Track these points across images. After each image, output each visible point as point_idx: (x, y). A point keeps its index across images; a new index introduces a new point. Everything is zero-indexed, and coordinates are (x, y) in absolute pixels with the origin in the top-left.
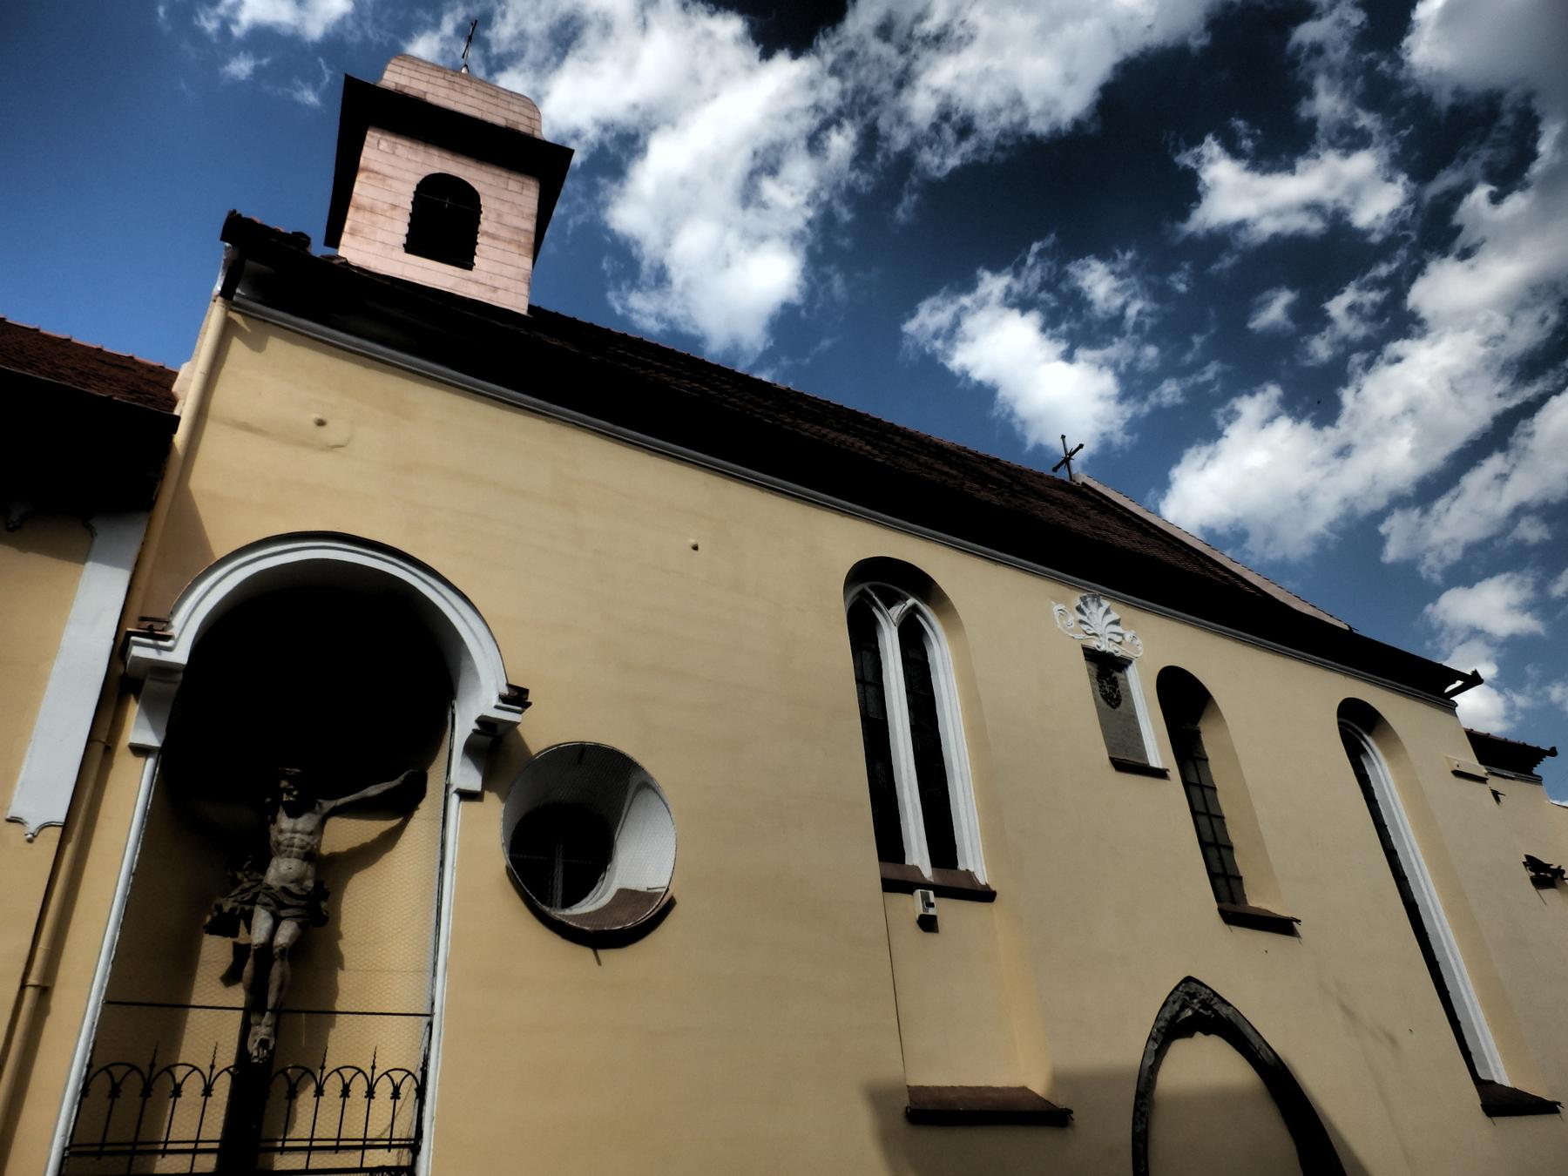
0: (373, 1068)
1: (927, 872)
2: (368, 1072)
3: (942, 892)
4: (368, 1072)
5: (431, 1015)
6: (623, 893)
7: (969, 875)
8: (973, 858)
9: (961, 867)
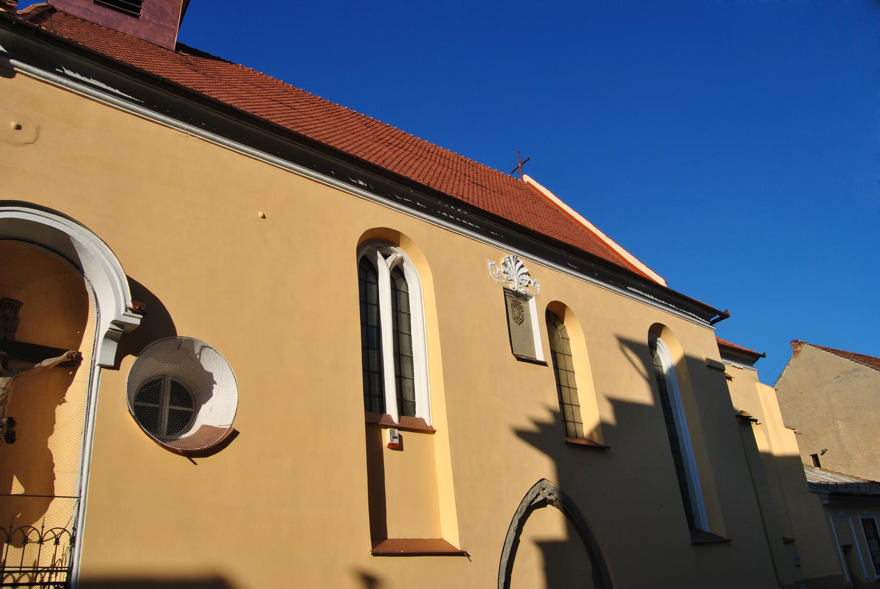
0: (43, 527)
1: (395, 419)
2: (40, 530)
3: (400, 429)
4: (40, 530)
5: (80, 497)
6: (203, 427)
7: (422, 420)
8: (421, 412)
9: (417, 416)
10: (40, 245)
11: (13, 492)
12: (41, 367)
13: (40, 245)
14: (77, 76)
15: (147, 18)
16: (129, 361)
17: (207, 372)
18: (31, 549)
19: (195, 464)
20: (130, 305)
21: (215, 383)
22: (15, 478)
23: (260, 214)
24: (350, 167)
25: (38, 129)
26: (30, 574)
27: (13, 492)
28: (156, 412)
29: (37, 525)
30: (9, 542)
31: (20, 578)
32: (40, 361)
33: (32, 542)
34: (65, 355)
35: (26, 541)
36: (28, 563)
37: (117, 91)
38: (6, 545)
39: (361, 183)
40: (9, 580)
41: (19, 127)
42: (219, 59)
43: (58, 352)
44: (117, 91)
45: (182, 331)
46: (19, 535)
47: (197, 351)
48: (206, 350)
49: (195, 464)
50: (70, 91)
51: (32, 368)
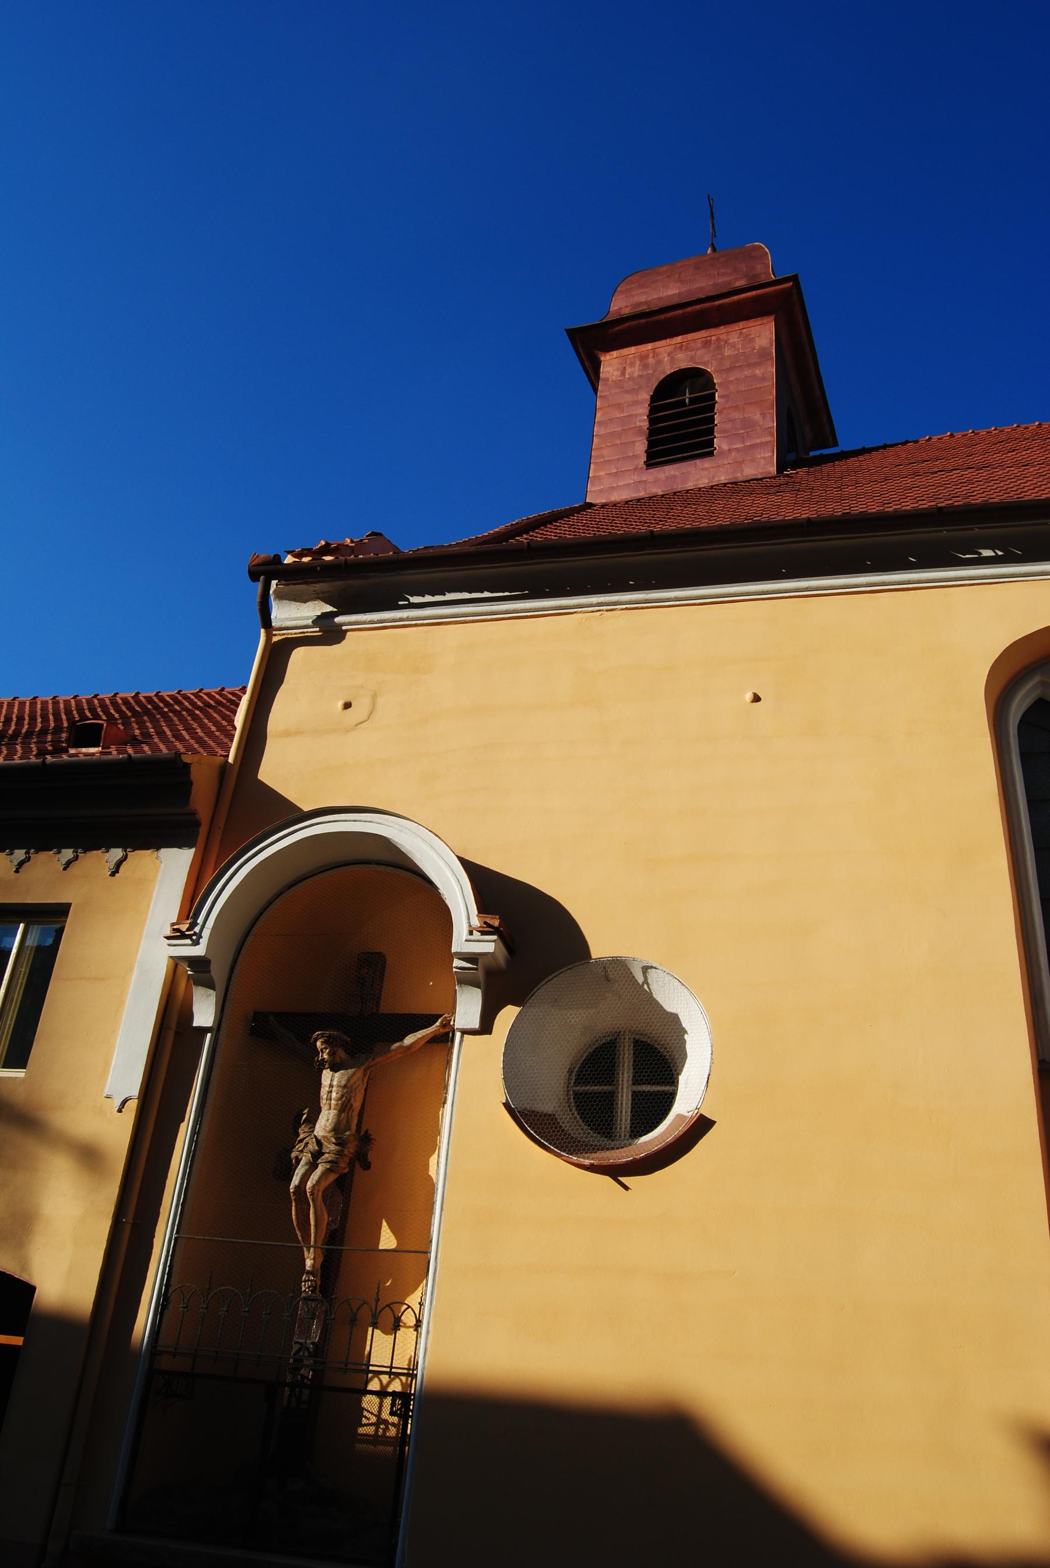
4: (373, 1303)
10: (378, 863)
11: (382, 1246)
12: (401, 1047)
13: (378, 863)
14: (428, 599)
15: (725, 447)
16: (507, 1016)
17: (672, 1014)
18: (405, 1335)
19: (626, 1188)
20: (476, 922)
21: (686, 1032)
22: (384, 1223)
23: (749, 696)
24: (945, 533)
25: (374, 697)
26: (403, 1378)
27: (382, 1246)
28: (609, 1100)
29: (413, 1300)
30: (375, 1326)
31: (389, 1383)
32: (402, 1039)
33: (405, 1326)
34: (438, 1024)
35: (396, 1325)
36: (401, 1362)
37: (486, 594)
38: (370, 1329)
39: (987, 553)
40: (374, 1385)
41: (347, 706)
42: (885, 447)
43: (428, 1020)
44: (486, 594)
45: (600, 948)
46: (387, 1317)
47: (640, 979)
48: (651, 971)
49: (626, 1188)
50: (416, 625)
51: (389, 1051)
